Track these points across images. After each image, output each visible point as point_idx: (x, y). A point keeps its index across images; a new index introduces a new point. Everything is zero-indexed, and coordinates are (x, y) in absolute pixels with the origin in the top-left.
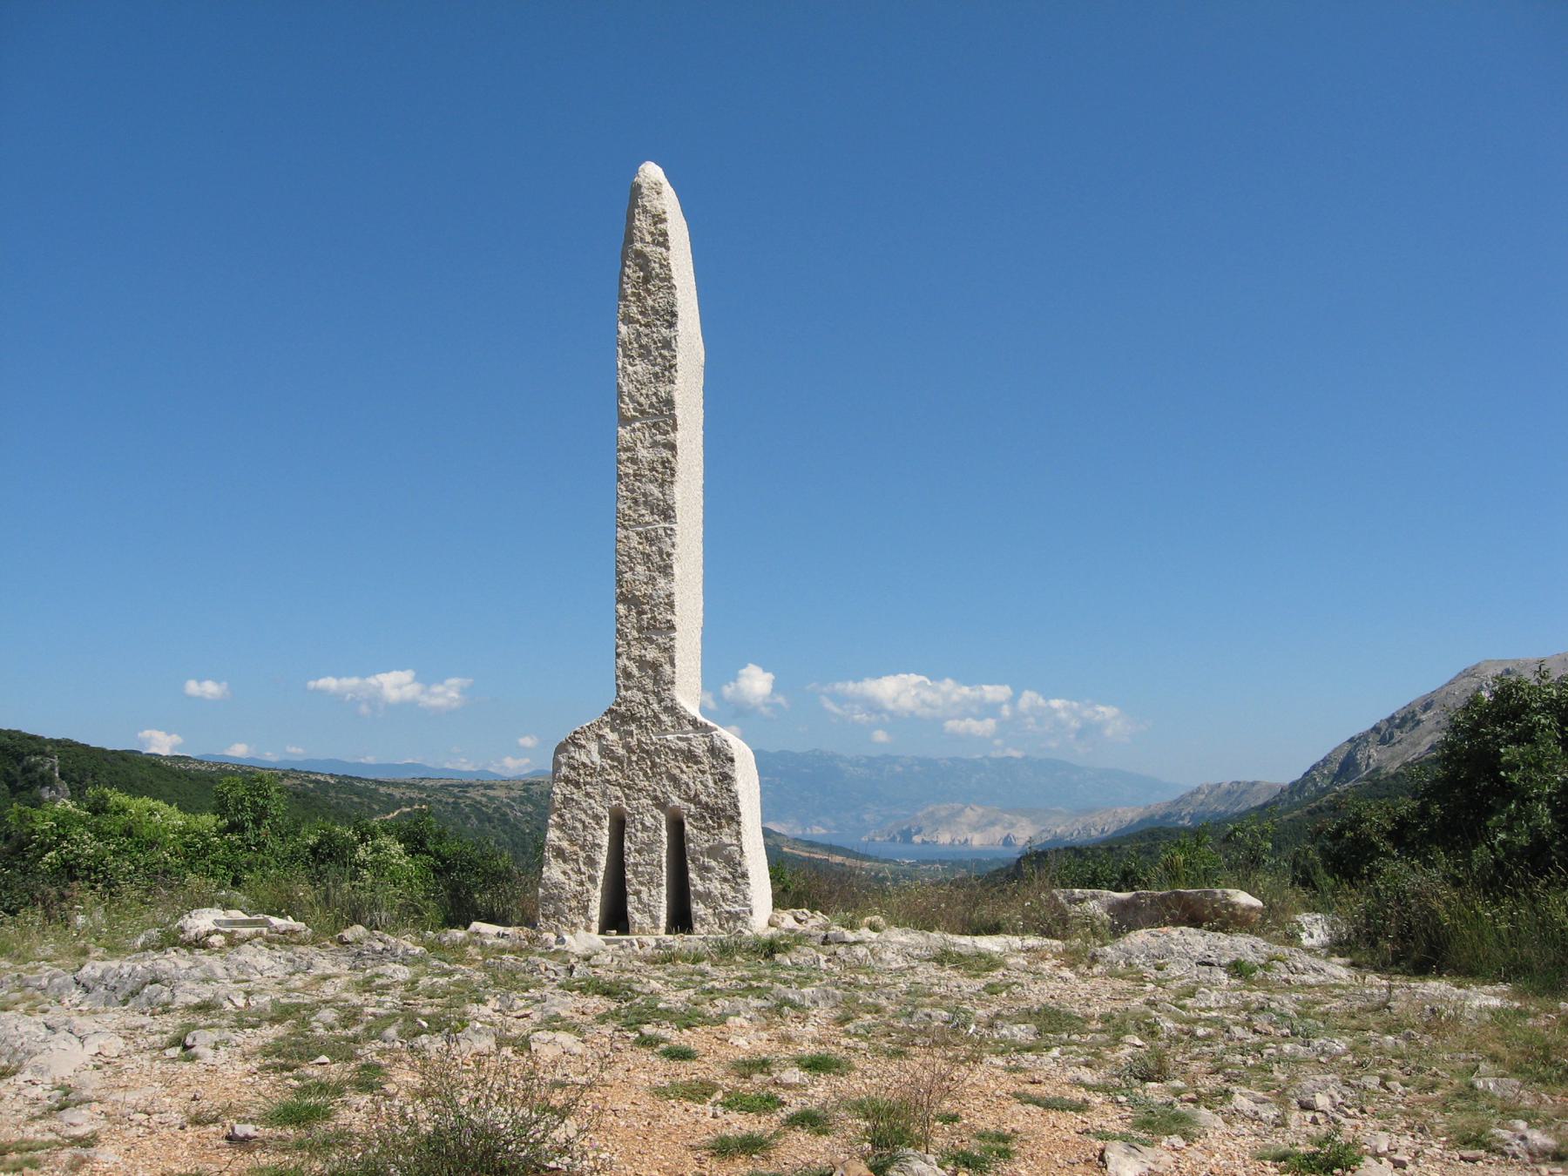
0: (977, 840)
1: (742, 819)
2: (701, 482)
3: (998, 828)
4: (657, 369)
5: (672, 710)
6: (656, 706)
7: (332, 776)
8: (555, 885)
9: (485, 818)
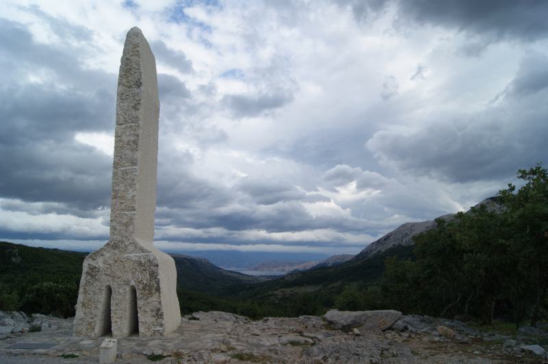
1: (161, 290)
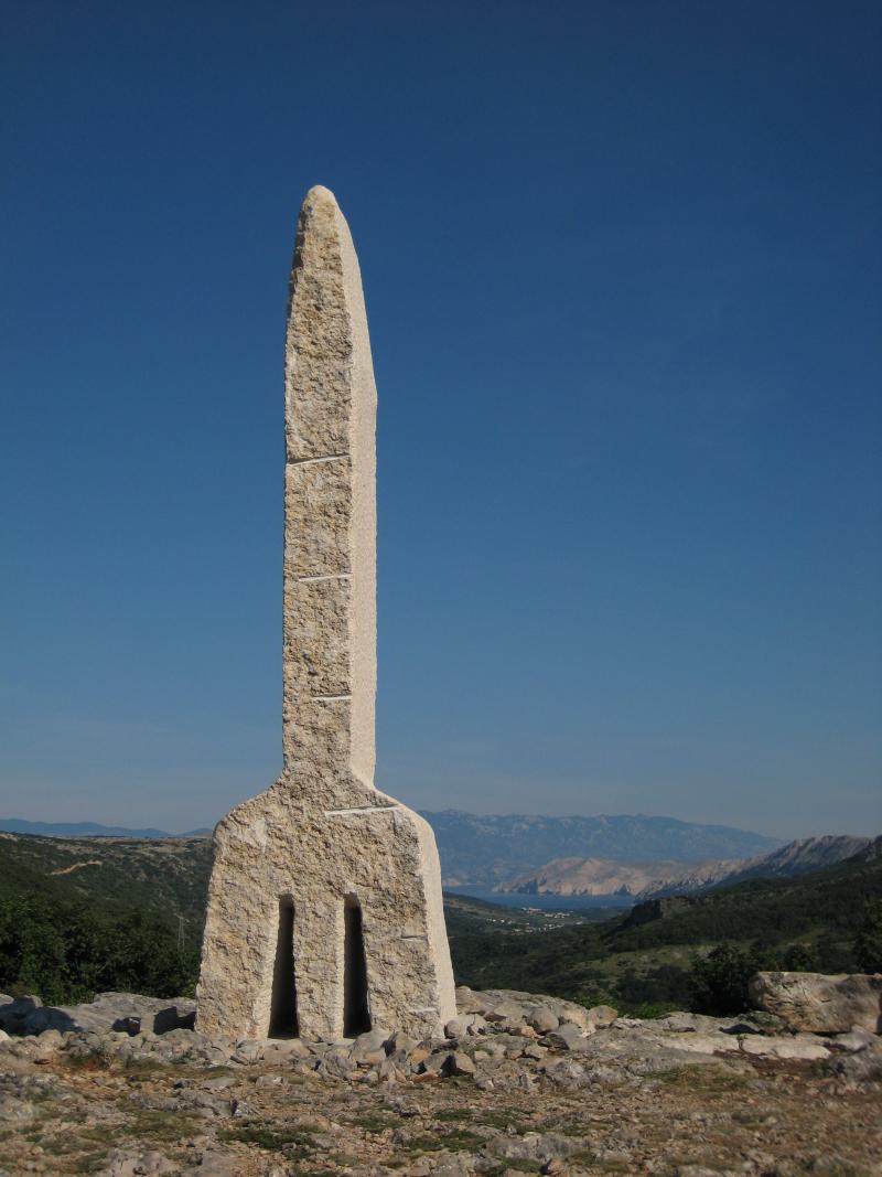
0: (596, 890)
1: (426, 907)
2: (375, 534)
3: (615, 880)
4: (329, 404)
5: (348, 782)
6: (329, 780)
7: (14, 834)
8: (217, 983)
9: (151, 872)
